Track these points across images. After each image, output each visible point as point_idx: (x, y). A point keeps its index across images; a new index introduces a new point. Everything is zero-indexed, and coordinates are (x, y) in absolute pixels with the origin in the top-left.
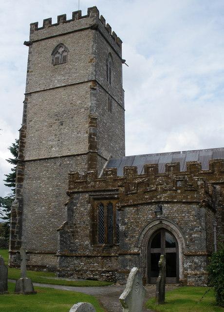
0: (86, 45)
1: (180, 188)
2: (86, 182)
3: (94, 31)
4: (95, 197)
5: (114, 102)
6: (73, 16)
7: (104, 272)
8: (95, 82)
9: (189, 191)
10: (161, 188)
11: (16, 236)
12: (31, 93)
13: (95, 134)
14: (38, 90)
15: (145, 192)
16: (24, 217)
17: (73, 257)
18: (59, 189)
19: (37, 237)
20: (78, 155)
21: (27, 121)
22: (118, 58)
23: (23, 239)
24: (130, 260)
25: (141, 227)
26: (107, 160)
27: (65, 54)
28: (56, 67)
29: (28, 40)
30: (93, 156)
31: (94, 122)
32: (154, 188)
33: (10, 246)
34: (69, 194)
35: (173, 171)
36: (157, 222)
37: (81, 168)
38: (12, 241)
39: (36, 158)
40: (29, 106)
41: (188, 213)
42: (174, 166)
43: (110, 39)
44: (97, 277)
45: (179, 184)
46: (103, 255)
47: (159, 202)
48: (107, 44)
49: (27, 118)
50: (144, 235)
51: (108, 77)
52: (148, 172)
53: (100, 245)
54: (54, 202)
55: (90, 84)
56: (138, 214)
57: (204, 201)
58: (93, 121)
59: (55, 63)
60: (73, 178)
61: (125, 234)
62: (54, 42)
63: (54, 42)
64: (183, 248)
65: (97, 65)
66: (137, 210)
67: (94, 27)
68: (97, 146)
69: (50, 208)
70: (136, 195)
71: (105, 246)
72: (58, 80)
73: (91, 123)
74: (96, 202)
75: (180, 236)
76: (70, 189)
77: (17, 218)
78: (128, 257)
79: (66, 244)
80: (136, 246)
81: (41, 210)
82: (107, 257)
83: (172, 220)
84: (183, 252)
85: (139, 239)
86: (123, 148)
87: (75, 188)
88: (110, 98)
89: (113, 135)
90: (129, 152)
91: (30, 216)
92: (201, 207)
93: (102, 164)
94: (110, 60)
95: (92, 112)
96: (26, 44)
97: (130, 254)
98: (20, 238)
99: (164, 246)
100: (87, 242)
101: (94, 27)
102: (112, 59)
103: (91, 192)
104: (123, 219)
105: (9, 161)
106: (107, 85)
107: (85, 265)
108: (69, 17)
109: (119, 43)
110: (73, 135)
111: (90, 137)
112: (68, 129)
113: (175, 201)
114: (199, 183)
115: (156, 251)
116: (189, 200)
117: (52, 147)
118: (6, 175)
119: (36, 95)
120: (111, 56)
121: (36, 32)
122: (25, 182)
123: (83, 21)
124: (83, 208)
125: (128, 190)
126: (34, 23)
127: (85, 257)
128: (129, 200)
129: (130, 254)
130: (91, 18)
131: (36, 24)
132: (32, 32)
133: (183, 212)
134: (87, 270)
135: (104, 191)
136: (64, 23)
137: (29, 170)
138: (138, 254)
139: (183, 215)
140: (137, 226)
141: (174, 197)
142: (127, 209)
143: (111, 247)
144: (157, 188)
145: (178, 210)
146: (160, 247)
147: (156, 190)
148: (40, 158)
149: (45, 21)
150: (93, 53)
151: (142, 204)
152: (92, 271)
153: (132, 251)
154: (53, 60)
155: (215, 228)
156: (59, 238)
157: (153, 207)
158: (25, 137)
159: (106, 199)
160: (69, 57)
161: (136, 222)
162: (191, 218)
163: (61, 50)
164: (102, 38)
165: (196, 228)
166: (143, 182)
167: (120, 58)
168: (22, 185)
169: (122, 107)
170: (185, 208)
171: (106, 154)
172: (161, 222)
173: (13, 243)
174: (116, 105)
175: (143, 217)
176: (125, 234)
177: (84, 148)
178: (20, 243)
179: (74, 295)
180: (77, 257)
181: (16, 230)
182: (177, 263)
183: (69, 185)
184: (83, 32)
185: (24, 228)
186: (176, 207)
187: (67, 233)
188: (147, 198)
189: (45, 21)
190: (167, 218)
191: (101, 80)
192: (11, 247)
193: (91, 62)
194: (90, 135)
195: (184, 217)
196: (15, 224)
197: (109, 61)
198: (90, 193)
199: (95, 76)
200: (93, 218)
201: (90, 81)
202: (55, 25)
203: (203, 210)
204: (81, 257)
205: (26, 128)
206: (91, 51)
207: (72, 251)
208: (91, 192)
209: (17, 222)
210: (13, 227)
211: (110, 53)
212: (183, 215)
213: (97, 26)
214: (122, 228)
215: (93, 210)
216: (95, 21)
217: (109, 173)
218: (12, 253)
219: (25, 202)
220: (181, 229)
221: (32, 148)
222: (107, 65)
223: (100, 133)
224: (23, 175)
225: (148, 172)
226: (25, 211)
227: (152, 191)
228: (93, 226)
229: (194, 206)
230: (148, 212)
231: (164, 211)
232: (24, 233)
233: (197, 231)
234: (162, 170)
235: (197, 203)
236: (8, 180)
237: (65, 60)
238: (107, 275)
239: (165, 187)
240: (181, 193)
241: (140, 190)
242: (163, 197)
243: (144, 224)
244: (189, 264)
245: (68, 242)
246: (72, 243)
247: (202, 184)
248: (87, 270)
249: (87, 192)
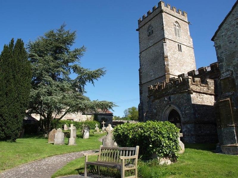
27: (152, 29)
62: (147, 26)
72: (151, 43)
76: (149, 94)
96: (137, 30)
108: (151, 11)
123: (157, 10)
224: (142, 91)
244: (185, 129)
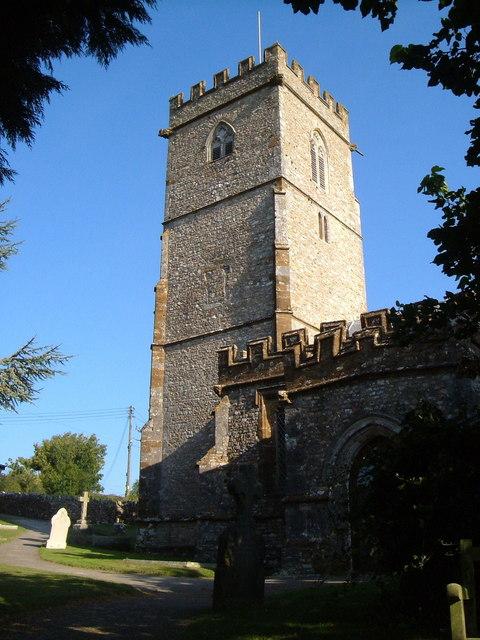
29: (168, 129)
78: (305, 508)
88: (324, 214)
94: (319, 143)
96: (163, 135)
102: (325, 143)
120: (322, 137)
129: (309, 501)
138: (325, 499)
179: (203, 589)
182: (32, 522)
197: (318, 145)
211: (318, 130)
222: (313, 153)
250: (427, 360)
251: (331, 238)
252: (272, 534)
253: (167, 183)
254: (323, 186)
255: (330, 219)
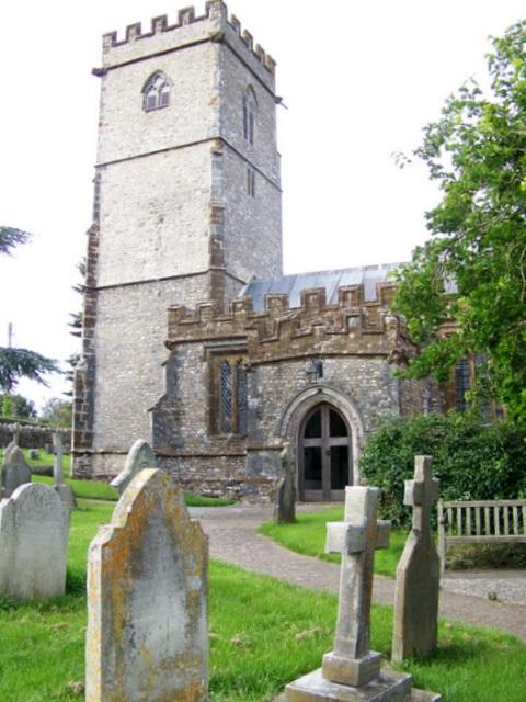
0: (202, 72)
1: (353, 330)
2: (198, 323)
3: (217, 45)
4: (215, 349)
5: (258, 176)
6: (180, 18)
7: (231, 484)
8: (220, 140)
9: (370, 336)
10: (321, 330)
11: (82, 424)
12: (106, 165)
13: (220, 237)
14: (119, 158)
15: (294, 338)
16: (97, 389)
17: (176, 457)
18: (157, 338)
19: (120, 425)
20: (191, 275)
21: (101, 216)
22: (267, 94)
23: (98, 429)
24: (267, 460)
25: (286, 401)
26: (244, 283)
28: (150, 114)
29: (99, 65)
30: (218, 272)
31: (220, 214)
32: (308, 332)
33: (73, 441)
34: (170, 345)
35: (352, 299)
36: (314, 392)
37: (195, 296)
38: (76, 433)
39: (118, 283)
40: (103, 187)
41: (368, 373)
42: (353, 292)
43: (250, 60)
44: (219, 492)
45: (352, 321)
46: (229, 453)
47: (317, 356)
48: (244, 70)
49: (101, 211)
50: (292, 415)
51: (247, 130)
52: (307, 303)
53: (223, 435)
54: (150, 360)
55: (212, 144)
56: (280, 378)
57: (395, 352)
58: (217, 213)
59: (149, 107)
60: (178, 316)
61: (258, 414)
62: (145, 69)
63: (145, 69)
64: (358, 438)
65: (223, 110)
66: (280, 370)
67: (218, 39)
68: (225, 259)
69: (141, 373)
70: (277, 343)
71: (233, 438)
73: (213, 216)
74: (216, 359)
75: (355, 415)
76: (170, 335)
77: (86, 390)
78: (263, 454)
79: (164, 433)
80: (277, 435)
81: (127, 375)
82: (237, 456)
83: (341, 388)
84: (359, 445)
85: (281, 422)
86: (278, 262)
87: (179, 334)
88: (252, 170)
89: (258, 238)
90: (290, 267)
91: (107, 388)
92: (391, 362)
93: (236, 291)
94: (251, 98)
95: (215, 197)
97: (267, 449)
98: (91, 427)
99: (328, 434)
100: (201, 431)
101: (218, 39)
103: (207, 340)
104: (255, 387)
105: (77, 289)
106: (246, 146)
107: (198, 471)
109: (270, 67)
110: (182, 240)
111: (212, 242)
112: (173, 230)
113: (345, 352)
114: (388, 320)
115: (312, 443)
116: (369, 352)
117: (145, 262)
118: (73, 315)
119: (117, 166)
120: (253, 92)
121: (113, 50)
122: (98, 325)
123: (198, 26)
124: (194, 373)
125: (264, 333)
126: (109, 35)
127: (197, 456)
128: (264, 353)
129: (267, 449)
130: (212, 20)
131: (113, 36)
132: (106, 49)
133: (358, 372)
134: (201, 481)
135: (230, 338)
136: (163, 31)
137: (106, 303)
139: (360, 378)
140: (279, 399)
141: (343, 347)
142: (261, 369)
143: (243, 438)
144: (313, 330)
145: (350, 369)
146: (320, 436)
147: (311, 334)
148: (124, 282)
149: (155, 21)
150: (215, 88)
151: (287, 360)
152: (209, 482)
153: (270, 444)
154: (144, 102)
155: (426, 402)
156: (151, 424)
157: (307, 365)
158: (97, 244)
159: (234, 353)
160: (173, 97)
161: (277, 392)
162: (374, 383)
163: (159, 82)
164: (233, 59)
165: (382, 401)
166: (288, 321)
167: (272, 94)
168: (92, 332)
169: (275, 185)
170: (363, 364)
171: (242, 273)
172: (320, 391)
173: (78, 435)
174: (264, 181)
175: (290, 382)
176: (258, 414)
177: (202, 262)
178: (90, 436)
180: (184, 457)
181: (82, 412)
183: (170, 329)
184: (197, 48)
185: (97, 409)
186: (347, 363)
187: (165, 416)
188: (296, 349)
189: (129, 28)
190: (331, 383)
191: (233, 138)
192: (75, 443)
193: (211, 104)
194: (212, 238)
195: (361, 381)
196: (82, 401)
198: (206, 344)
199: (221, 129)
200: (212, 388)
201: (211, 139)
202: (149, 35)
203: (394, 368)
204: (190, 457)
205: (98, 230)
206: (212, 83)
207: (174, 447)
208: (207, 340)
209: (85, 398)
210: (78, 408)
212: (360, 378)
213: (223, 36)
214: (253, 402)
215: (211, 374)
216: (219, 27)
217: (239, 306)
218: (76, 454)
219: (100, 361)
220: (355, 402)
221: (109, 265)
222: (245, 109)
223: (230, 234)
225: (307, 303)
226: (100, 378)
227: (306, 335)
228: (213, 402)
229: (379, 361)
230: (297, 374)
231: (325, 372)
232: (98, 418)
233: (383, 407)
234: (331, 298)
235: (384, 356)
236: (77, 325)
237: (165, 100)
238: (236, 488)
239: (328, 329)
240: (356, 338)
241: (285, 335)
242: (324, 346)
243: (291, 395)
245: (168, 432)
246: (174, 433)
247: (392, 322)
248: (201, 481)
249: (200, 341)
250: (366, 348)
251: (257, 193)
252: (216, 470)
253: (100, 125)
254: (251, 142)
255: (258, 176)
